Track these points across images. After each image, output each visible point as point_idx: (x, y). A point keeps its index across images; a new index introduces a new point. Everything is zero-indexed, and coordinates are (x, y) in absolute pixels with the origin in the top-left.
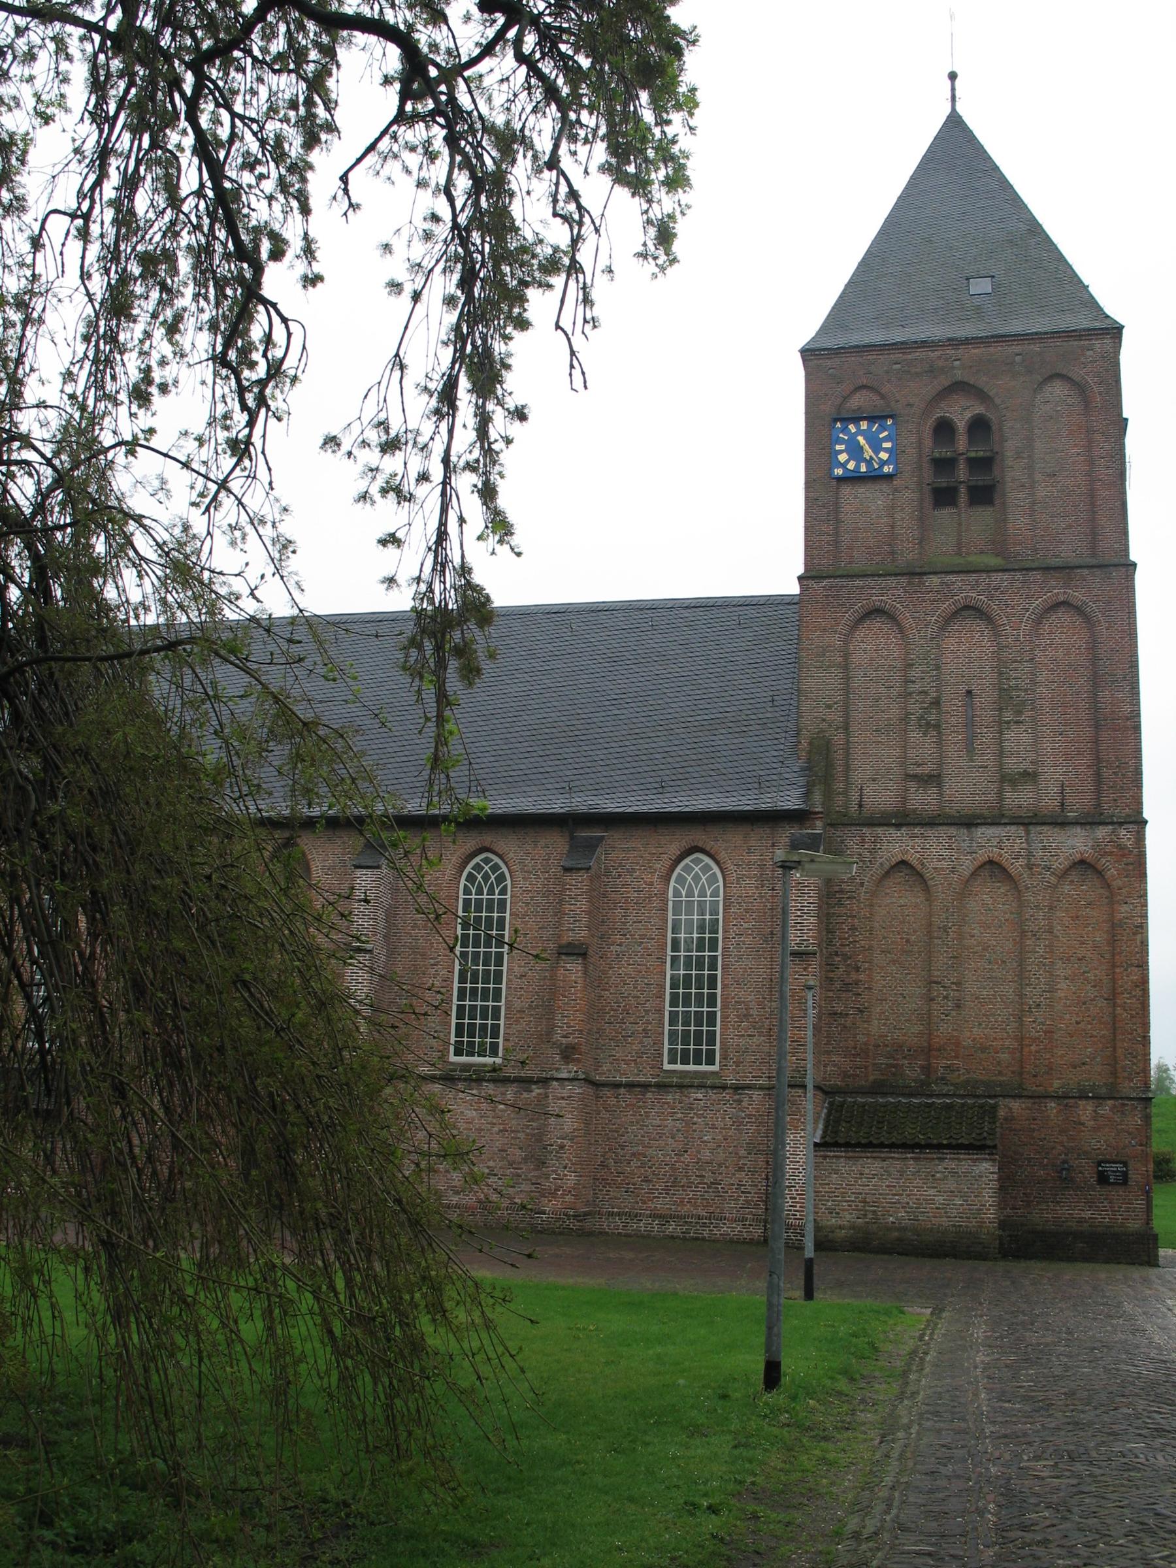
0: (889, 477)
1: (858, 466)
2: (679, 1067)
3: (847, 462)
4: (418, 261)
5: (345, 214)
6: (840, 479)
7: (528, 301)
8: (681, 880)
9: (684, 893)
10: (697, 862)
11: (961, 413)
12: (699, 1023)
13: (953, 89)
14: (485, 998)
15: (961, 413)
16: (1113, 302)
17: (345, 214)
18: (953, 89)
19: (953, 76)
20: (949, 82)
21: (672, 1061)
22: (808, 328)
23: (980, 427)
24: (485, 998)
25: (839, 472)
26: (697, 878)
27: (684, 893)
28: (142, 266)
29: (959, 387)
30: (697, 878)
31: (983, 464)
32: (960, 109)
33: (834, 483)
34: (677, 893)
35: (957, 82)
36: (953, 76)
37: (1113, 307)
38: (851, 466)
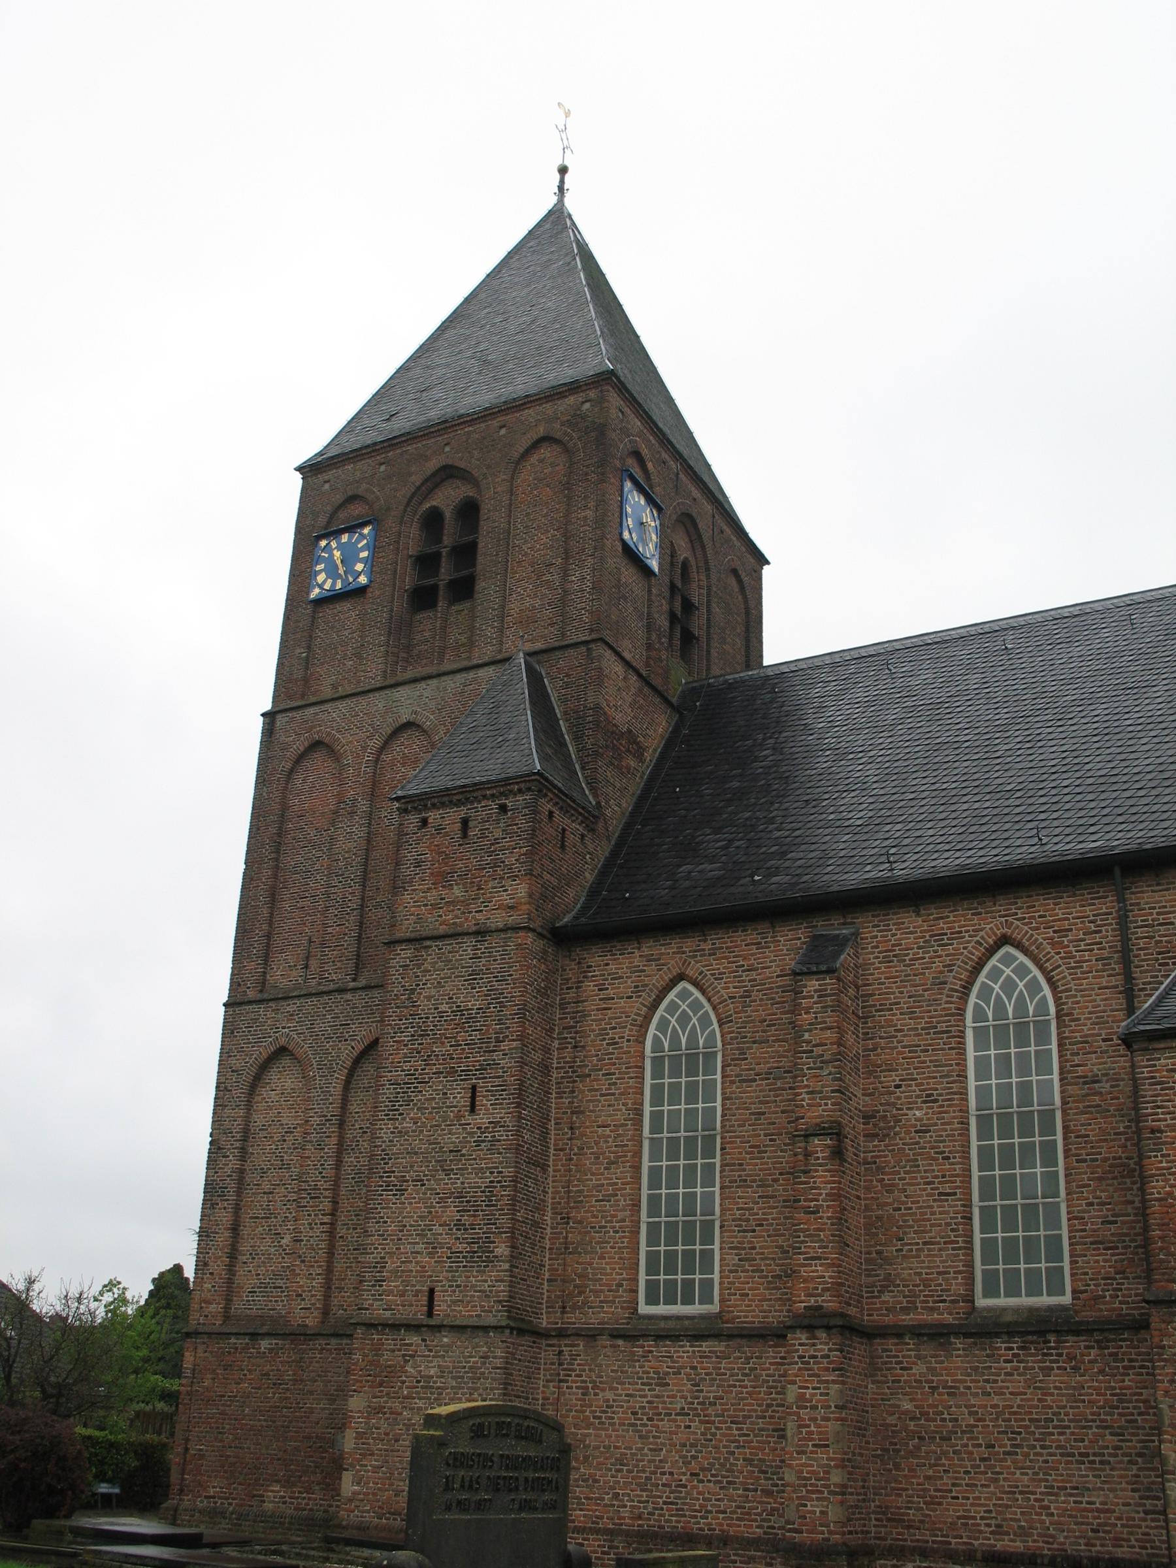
1: (334, 584)
2: (661, 1309)
3: (324, 582)
5: (567, 114)
6: (319, 602)
8: (985, 993)
9: (666, 1045)
10: (1007, 960)
15: (447, 498)
17: (567, 114)
18: (562, 182)
19: (563, 170)
20: (558, 177)
21: (652, 1300)
22: (315, 438)
26: (1009, 987)
27: (666, 1045)
29: (448, 473)
30: (1009, 987)
32: (570, 204)
34: (979, 1015)
35: (567, 177)
36: (563, 170)
37: (296, 482)
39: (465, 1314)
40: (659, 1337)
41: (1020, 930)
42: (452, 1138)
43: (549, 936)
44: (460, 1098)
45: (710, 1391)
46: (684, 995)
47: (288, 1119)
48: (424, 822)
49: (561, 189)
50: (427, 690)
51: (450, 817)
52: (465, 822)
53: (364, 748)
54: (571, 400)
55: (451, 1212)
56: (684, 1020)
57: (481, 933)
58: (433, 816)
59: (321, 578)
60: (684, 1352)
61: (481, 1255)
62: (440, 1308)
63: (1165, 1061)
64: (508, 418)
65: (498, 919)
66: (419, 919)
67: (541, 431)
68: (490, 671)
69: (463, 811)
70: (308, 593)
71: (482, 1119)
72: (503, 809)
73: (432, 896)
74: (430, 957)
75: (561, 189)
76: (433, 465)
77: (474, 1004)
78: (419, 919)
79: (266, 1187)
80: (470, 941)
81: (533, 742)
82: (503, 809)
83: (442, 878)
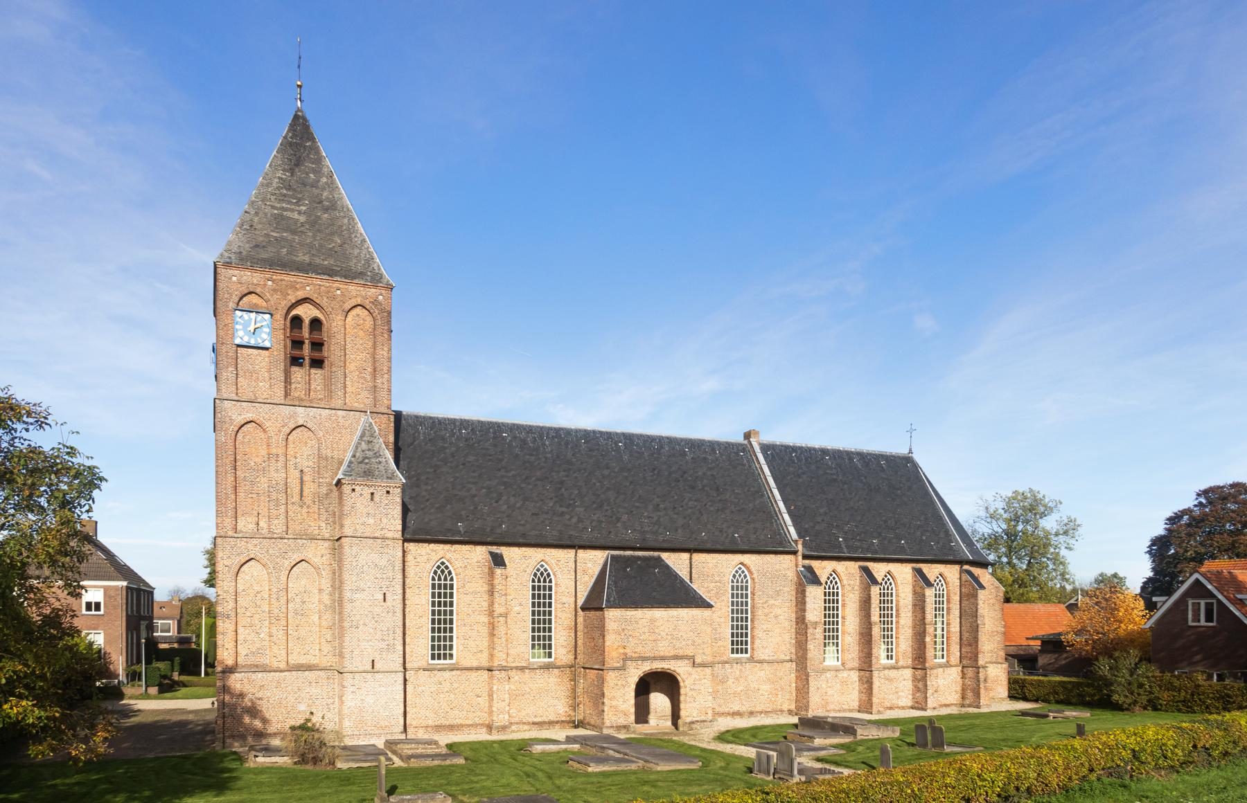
25: (238, 341)
45: (455, 685)
56: (443, 572)
59: (241, 333)
62: (377, 666)
65: (390, 535)
70: (233, 336)
72: (388, 492)
76: (301, 294)
79: (248, 614)
82: (388, 492)
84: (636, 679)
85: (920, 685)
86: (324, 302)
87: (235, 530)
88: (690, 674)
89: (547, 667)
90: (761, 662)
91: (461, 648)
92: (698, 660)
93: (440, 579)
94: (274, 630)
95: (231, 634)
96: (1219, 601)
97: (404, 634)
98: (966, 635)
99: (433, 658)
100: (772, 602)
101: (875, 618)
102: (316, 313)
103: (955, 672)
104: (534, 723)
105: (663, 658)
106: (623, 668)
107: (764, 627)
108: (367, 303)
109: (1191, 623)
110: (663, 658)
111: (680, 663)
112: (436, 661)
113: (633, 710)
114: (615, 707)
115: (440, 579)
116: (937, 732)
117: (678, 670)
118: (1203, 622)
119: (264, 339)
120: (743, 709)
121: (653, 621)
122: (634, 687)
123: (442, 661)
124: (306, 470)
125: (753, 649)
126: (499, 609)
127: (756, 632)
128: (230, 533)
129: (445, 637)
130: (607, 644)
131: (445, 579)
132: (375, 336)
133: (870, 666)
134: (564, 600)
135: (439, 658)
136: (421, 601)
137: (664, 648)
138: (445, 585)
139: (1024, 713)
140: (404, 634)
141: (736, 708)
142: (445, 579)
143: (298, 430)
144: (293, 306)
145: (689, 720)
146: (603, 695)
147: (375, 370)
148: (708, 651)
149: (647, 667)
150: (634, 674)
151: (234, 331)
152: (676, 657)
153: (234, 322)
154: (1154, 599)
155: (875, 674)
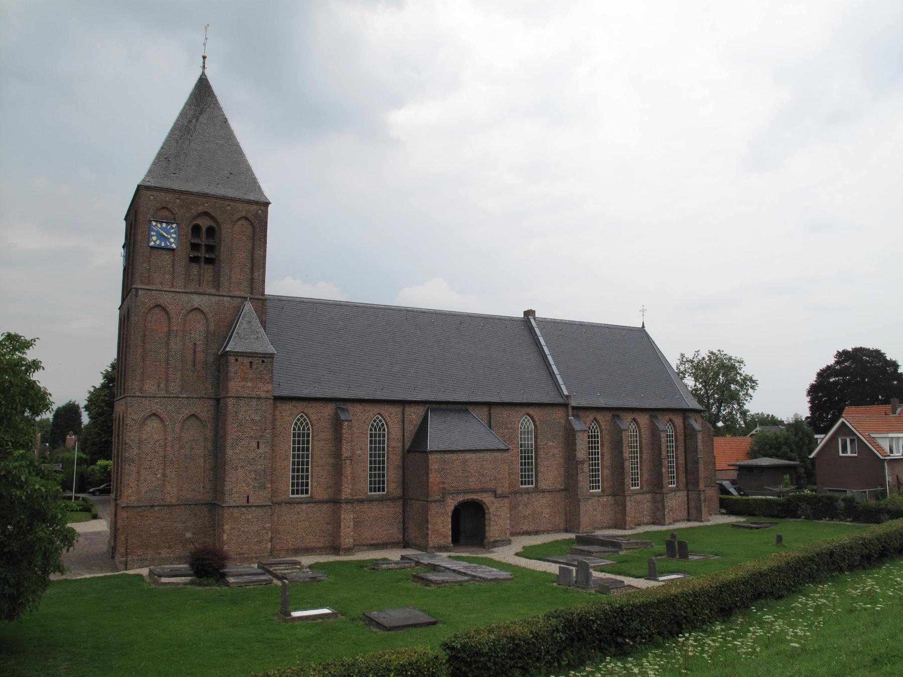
0: (173, 250)
4: (691, 358)
6: (152, 247)
7: (749, 382)
11: (204, 223)
12: (379, 477)
13: (204, 63)
14: (375, 474)
15: (204, 223)
16: (269, 188)
18: (204, 63)
19: (204, 58)
21: (293, 493)
23: (211, 231)
24: (375, 474)
25: (152, 244)
28: (815, 407)
29: (206, 214)
31: (210, 248)
32: (206, 72)
33: (149, 249)
36: (204, 58)
38: (158, 242)
39: (258, 503)
40: (298, 503)
41: (382, 413)
42: (253, 455)
43: (407, 447)
44: (255, 445)
45: (310, 515)
46: (302, 417)
47: (156, 437)
48: (237, 360)
49: (204, 67)
50: (205, 298)
51: (246, 361)
52: (251, 363)
53: (180, 313)
54: (255, 207)
55: (253, 476)
56: (302, 423)
57: (259, 398)
58: (240, 359)
59: (154, 238)
60: (304, 507)
61: (262, 486)
62: (251, 500)
63: (434, 456)
64: (232, 204)
65: (263, 395)
66: (237, 390)
67: (244, 214)
68: (228, 299)
69: (250, 360)
70: (149, 242)
71: (261, 451)
72: (263, 361)
73: (241, 384)
74: (242, 403)
75: (204, 67)
76: (201, 209)
77: (257, 418)
78: (237, 390)
79: (149, 458)
80: (254, 402)
81: (641, 530)
82: (263, 361)
83: (245, 379)
84: (452, 508)
85: (659, 505)
86: (217, 215)
87: (141, 390)
88: (493, 503)
89: (381, 500)
90: (543, 491)
91: (315, 484)
92: (499, 491)
93: (299, 429)
94: (168, 471)
95: (134, 476)
96: (858, 437)
97: (452, 452)
98: (690, 466)
99: (293, 493)
100: (550, 444)
101: (581, 453)
102: (210, 223)
103: (682, 495)
104: (371, 545)
105: (473, 492)
106: (442, 500)
107: (545, 463)
108: (250, 216)
109: (841, 454)
110: (473, 492)
111: (485, 495)
112: (296, 496)
113: (450, 533)
114: (437, 530)
115: (299, 429)
116: (683, 545)
117: (485, 500)
118: (849, 454)
119: (173, 243)
120: (531, 529)
121: (465, 461)
122: (450, 514)
123: (300, 496)
124: (198, 343)
125: (537, 481)
126: (346, 453)
127: (541, 469)
128: (138, 394)
129: (375, 464)
130: (431, 480)
131: (304, 429)
132: (254, 240)
133: (624, 492)
134: (395, 444)
135: (298, 493)
136: (287, 446)
137: (473, 483)
138: (303, 434)
139: (734, 526)
140: (452, 452)
141: (525, 528)
142: (304, 429)
143: (194, 312)
144: (195, 218)
145: (492, 540)
146: (427, 521)
147: (253, 266)
148: (506, 485)
149: (461, 498)
150: (451, 504)
151: (150, 236)
152: (483, 491)
153: (150, 230)
154: (816, 436)
155: (628, 499)
